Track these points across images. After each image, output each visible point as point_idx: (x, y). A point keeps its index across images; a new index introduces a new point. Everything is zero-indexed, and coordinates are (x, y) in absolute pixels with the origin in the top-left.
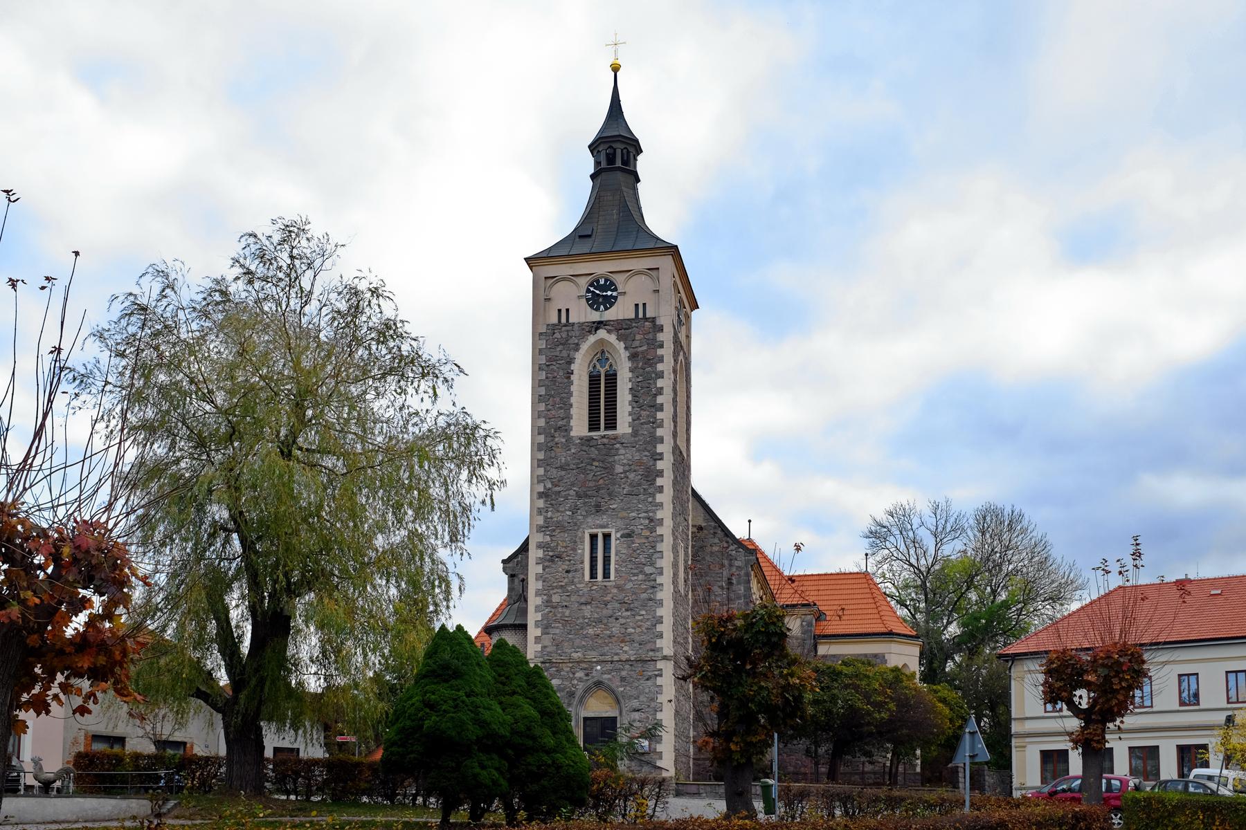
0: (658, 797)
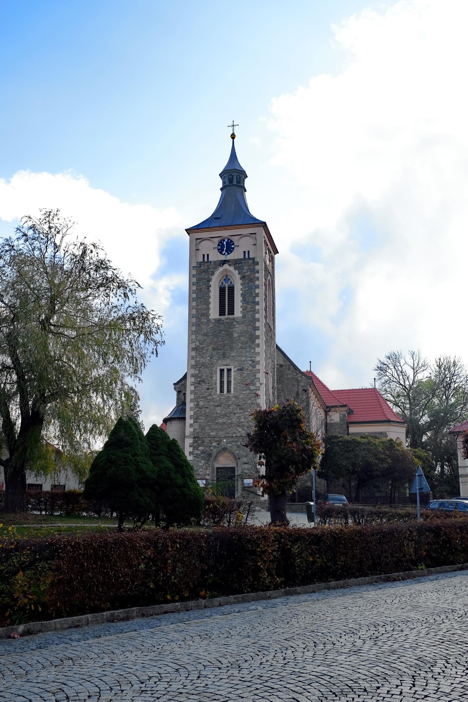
0: (249, 512)
